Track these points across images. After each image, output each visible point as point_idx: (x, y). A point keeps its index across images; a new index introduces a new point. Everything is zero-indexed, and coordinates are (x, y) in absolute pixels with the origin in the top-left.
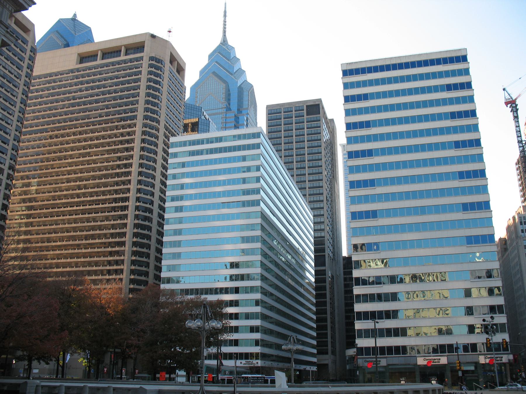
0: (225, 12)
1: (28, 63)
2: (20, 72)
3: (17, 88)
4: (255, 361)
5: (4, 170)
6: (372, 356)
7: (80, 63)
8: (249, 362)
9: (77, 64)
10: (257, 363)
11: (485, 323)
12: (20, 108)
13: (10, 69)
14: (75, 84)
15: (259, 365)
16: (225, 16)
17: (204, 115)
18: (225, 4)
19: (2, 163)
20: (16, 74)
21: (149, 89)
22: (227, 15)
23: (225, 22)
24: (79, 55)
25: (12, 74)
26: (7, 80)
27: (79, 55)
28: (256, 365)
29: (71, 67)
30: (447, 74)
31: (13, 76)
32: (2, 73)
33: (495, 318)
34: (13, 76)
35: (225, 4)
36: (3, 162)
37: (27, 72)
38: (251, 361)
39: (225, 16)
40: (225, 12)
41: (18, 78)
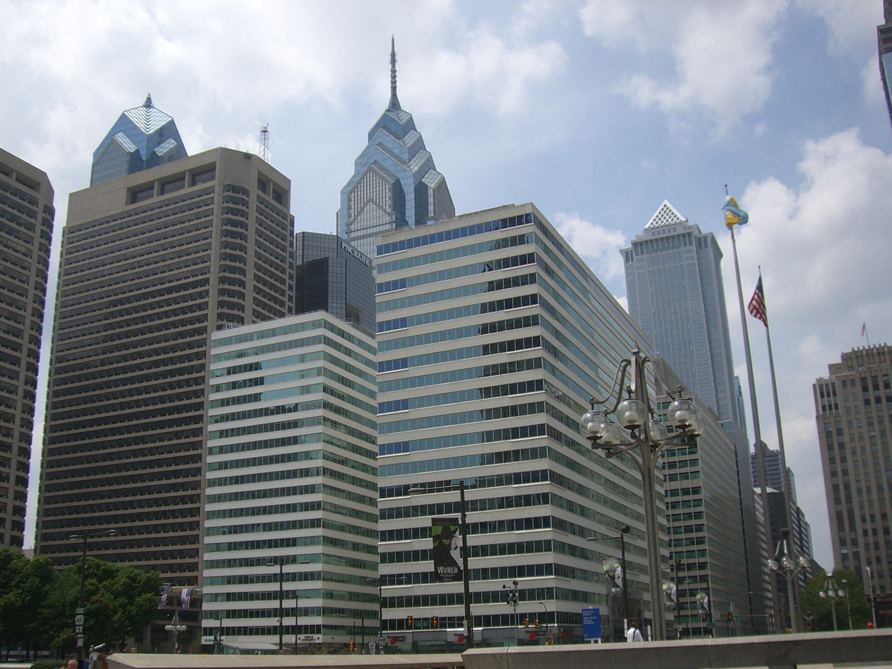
0: (393, 55)
1: (42, 230)
2: (29, 246)
3: (28, 270)
4: (315, 636)
5: (35, 225)
6: (554, 577)
7: (132, 203)
8: (309, 637)
9: (127, 204)
10: (318, 638)
11: (506, 589)
12: (23, 406)
13: (14, 245)
14: (105, 317)
15: (321, 641)
16: (393, 61)
17: (343, 247)
18: (393, 40)
19: (2, 496)
20: (24, 250)
21: (223, 271)
22: (397, 58)
23: (394, 71)
24: (129, 189)
25: (18, 252)
26: (12, 263)
27: (129, 189)
28: (317, 641)
29: (120, 210)
30: (230, 563)
31: (20, 255)
32: (1, 268)
33: (519, 583)
34: (20, 255)
35: (393, 40)
36: (3, 494)
37: (41, 244)
38: (311, 635)
39: (393, 61)
40: (393, 55)
41: (27, 256)
